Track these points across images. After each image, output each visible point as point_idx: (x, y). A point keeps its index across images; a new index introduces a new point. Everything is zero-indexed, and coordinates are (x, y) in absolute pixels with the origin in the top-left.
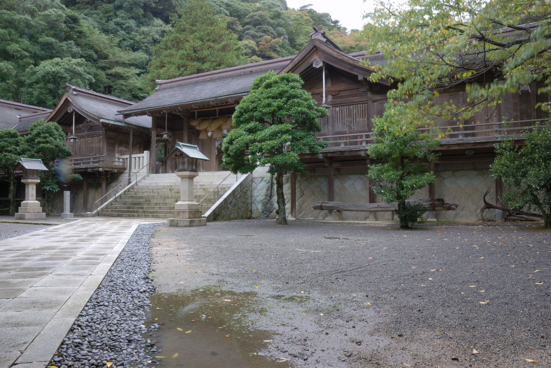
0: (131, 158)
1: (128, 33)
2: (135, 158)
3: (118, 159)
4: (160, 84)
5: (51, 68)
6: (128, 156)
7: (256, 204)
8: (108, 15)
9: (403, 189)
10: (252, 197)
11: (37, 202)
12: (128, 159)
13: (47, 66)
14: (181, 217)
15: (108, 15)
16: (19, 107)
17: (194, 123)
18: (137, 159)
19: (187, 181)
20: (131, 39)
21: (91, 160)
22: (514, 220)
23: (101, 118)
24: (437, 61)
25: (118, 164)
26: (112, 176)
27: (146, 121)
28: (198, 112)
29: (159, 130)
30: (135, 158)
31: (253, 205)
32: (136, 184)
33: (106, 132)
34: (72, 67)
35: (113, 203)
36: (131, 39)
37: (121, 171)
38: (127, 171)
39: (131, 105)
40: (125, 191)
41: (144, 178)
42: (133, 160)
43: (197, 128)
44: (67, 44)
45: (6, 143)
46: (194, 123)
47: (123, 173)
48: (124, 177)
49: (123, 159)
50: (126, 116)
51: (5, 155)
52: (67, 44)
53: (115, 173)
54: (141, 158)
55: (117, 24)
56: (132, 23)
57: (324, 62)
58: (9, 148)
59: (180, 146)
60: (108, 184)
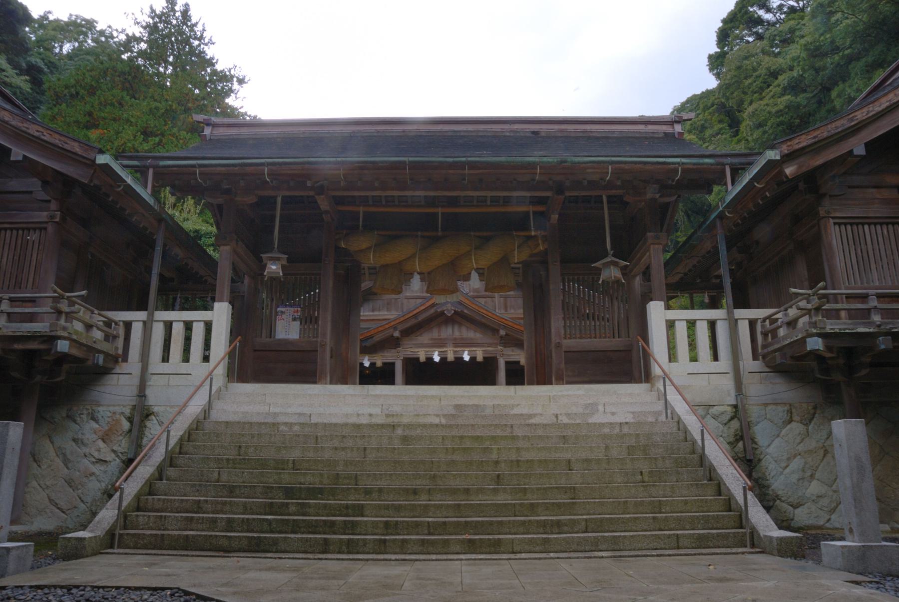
6: (142, 315)
17: (359, 243)
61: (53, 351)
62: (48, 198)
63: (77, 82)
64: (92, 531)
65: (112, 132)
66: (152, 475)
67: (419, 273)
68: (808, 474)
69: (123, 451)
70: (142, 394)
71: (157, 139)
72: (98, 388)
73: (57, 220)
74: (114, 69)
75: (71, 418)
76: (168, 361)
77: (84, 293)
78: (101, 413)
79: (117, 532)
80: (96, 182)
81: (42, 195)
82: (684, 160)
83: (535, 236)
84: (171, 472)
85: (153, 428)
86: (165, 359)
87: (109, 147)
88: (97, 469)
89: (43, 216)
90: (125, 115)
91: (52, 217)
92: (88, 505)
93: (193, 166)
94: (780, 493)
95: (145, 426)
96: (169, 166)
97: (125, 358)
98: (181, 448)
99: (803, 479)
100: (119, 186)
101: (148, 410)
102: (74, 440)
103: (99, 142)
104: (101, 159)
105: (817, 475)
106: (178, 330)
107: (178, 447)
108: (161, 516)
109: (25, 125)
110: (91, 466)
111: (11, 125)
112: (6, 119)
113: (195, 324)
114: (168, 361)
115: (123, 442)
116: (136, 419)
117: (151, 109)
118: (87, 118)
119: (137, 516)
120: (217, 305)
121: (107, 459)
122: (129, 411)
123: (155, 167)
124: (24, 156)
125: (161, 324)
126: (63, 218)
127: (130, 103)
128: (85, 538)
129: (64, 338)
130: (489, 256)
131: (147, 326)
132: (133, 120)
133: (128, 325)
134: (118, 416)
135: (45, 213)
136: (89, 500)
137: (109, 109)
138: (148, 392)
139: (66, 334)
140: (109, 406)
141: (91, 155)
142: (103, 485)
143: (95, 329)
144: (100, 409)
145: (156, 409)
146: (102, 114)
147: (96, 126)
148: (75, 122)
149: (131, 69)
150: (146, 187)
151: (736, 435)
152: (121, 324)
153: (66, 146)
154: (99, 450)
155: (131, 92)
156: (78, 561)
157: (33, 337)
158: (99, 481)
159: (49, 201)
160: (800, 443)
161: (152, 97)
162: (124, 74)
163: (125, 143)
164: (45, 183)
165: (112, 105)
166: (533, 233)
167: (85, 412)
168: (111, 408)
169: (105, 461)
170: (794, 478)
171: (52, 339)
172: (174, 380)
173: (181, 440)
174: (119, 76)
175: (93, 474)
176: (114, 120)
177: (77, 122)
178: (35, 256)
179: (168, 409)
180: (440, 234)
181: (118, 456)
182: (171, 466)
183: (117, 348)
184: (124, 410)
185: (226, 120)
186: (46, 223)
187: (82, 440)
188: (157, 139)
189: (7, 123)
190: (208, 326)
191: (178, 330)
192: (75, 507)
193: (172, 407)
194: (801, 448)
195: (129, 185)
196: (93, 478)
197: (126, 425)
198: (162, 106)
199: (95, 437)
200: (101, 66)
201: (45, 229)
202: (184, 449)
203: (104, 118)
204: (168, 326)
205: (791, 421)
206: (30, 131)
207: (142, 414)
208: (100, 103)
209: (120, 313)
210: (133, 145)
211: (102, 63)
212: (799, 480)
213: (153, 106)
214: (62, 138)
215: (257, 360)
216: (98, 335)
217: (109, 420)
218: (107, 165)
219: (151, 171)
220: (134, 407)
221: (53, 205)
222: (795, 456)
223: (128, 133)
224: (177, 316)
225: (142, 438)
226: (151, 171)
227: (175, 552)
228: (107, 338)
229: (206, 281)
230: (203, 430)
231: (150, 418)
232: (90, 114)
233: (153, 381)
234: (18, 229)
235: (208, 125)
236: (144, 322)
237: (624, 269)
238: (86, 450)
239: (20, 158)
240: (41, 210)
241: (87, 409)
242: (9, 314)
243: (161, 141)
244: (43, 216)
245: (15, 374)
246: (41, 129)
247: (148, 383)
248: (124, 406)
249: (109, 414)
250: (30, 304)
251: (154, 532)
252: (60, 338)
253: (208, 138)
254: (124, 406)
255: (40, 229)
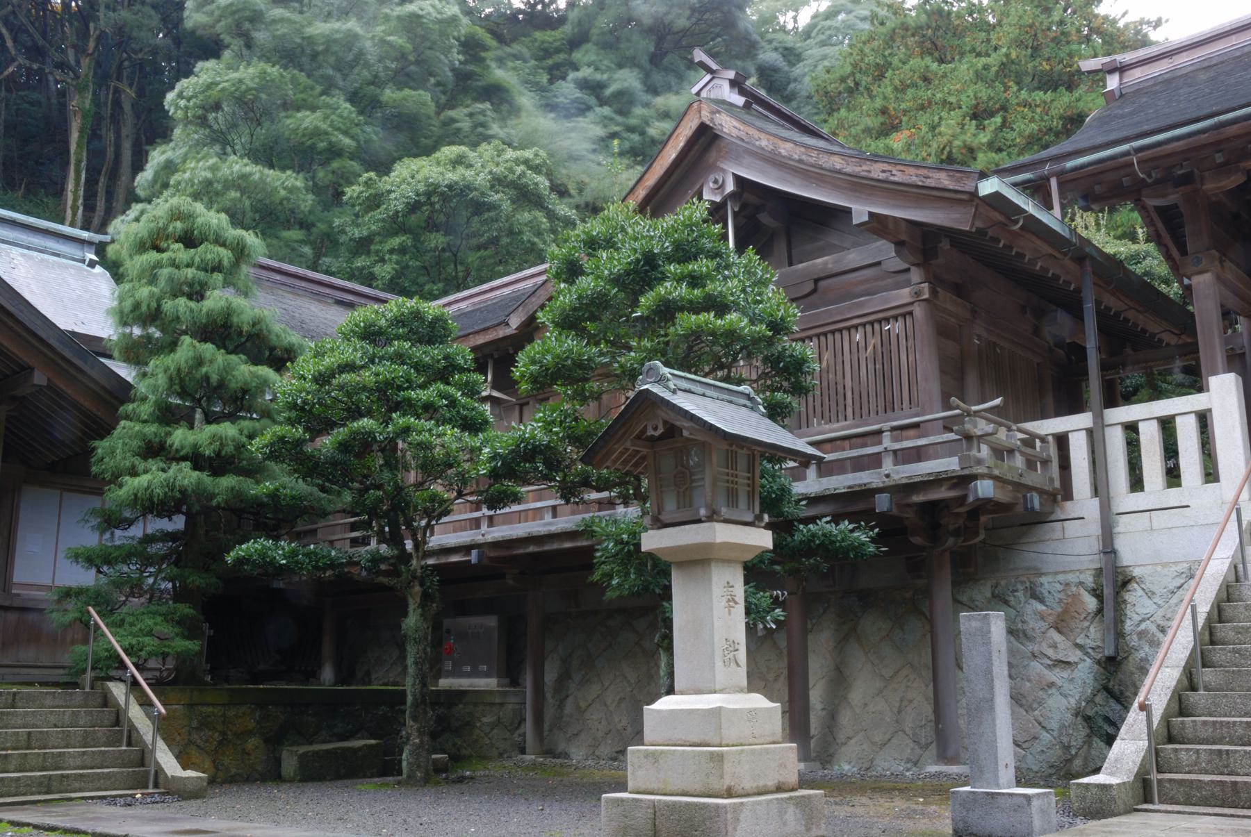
1: (621, 112)
5: (442, 174)
6: (1083, 420)
8: (550, 62)
9: (1193, 688)
11: (759, 701)
13: (410, 176)
15: (550, 62)
16: (351, 298)
20: (631, 129)
21: (887, 442)
24: (963, 423)
34: (511, 170)
36: (631, 129)
44: (471, 115)
45: (401, 370)
51: (407, 430)
52: (471, 115)
55: (585, 85)
56: (628, 79)
58: (423, 395)
61: (971, 499)
62: (906, 266)
63: (855, 65)
64: (1112, 774)
65: (925, 129)
66: (1179, 681)
69: (1094, 644)
70: (1109, 550)
71: (998, 120)
72: (1034, 548)
73: (926, 296)
74: (905, 28)
76: (1142, 489)
77: (998, 401)
78: (1047, 586)
79: (1154, 776)
80: (979, 224)
81: (899, 264)
84: (1207, 676)
85: (1139, 605)
86: (1137, 483)
87: (924, 154)
88: (1056, 676)
89: (904, 295)
90: (939, 96)
91: (917, 294)
92: (1055, 734)
93: (1127, 154)
95: (1125, 602)
96: (1083, 167)
97: (1067, 494)
98: (1211, 634)
100: (1016, 222)
101: (1124, 573)
103: (908, 150)
104: (988, 187)
106: (1150, 437)
107: (1207, 633)
108: (1220, 751)
109: (864, 168)
110: (1046, 672)
111: (846, 174)
112: (838, 167)
113: (1178, 420)
114: (1142, 489)
115: (1092, 629)
116: (1108, 592)
117: (977, 74)
118: (881, 119)
119: (1176, 750)
120: (1214, 381)
121: (1070, 659)
122: (1091, 579)
123: (1059, 174)
124: (871, 214)
125: (1119, 429)
126: (933, 292)
127: (940, 73)
128: (1111, 786)
129: (983, 476)
131: (1095, 438)
132: (952, 99)
133: (1062, 440)
134: (1074, 589)
135: (907, 290)
136: (1054, 725)
137: (910, 92)
138: (1121, 544)
139: (985, 471)
140: (1056, 573)
141: (969, 187)
142: (1073, 701)
143: (1017, 454)
144: (1043, 580)
145: (1136, 572)
146: (903, 106)
147: (895, 128)
148: (864, 131)
149: (929, 16)
150: (1048, 206)
152: (1050, 438)
153: (928, 183)
154: (1054, 646)
155: (936, 54)
156: (1103, 821)
157: (937, 481)
158: (1066, 696)
159: (908, 270)
161: (973, 50)
162: (921, 28)
163: (950, 142)
164: (899, 244)
165: (914, 85)
167: (1020, 587)
168: (1061, 577)
169: (1068, 663)
171: (963, 481)
172: (1160, 519)
173: (1209, 619)
174: (913, 35)
175: (1052, 685)
176: (922, 108)
177: (867, 131)
178: (904, 357)
179: (1159, 568)
181: (1087, 654)
182: (1204, 666)
183: (1052, 480)
184: (1082, 577)
185: (1142, 53)
186: (912, 303)
187: (1024, 632)
188: (998, 120)
189: (839, 172)
190: (1204, 419)
191: (1150, 437)
192: (1035, 738)
193: (1165, 565)
194: (948, 149)
195: (1032, 216)
196: (1054, 690)
197: (1091, 603)
198: (994, 60)
199: (1042, 625)
200: (882, 30)
201: (911, 313)
202: (1219, 635)
203: (905, 112)
204: (1131, 428)
206: (874, 175)
207: (1114, 583)
208: (896, 89)
209: (1044, 421)
210: (964, 142)
211: (882, 24)
213: (980, 66)
214: (921, 172)
216: (1019, 461)
217: (1062, 596)
218: (997, 195)
219: (1054, 183)
220: (1099, 573)
221: (916, 275)
223: (949, 124)
224: (1144, 412)
225: (1123, 622)
226: (1054, 183)
227: (1210, 810)
228: (1031, 464)
229: (1161, 341)
230: (1241, 600)
231: (1129, 587)
232: (884, 111)
233: (1124, 525)
234: (872, 323)
235: (1111, 72)
236: (1090, 432)
238: (1031, 647)
239: (866, 218)
240: (899, 286)
241: (1022, 583)
242: (895, 452)
243: (1004, 120)
244: (904, 295)
245: (917, 540)
246: (886, 167)
247: (1116, 530)
248: (1081, 572)
249: (1060, 587)
250: (911, 432)
251: (1219, 778)
253: (1117, 94)
255: (904, 315)
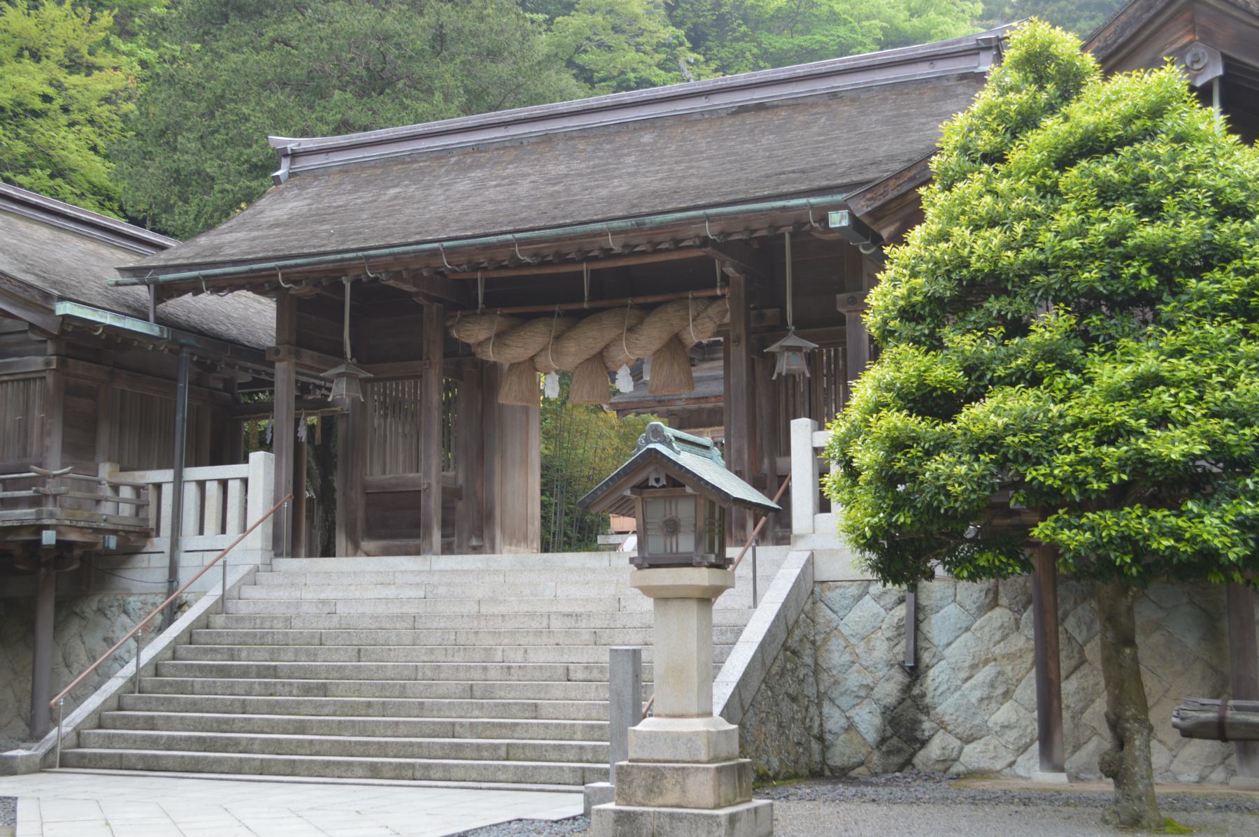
0: (179, 483)
2: (201, 484)
3: (117, 489)
4: (294, 155)
6: (165, 476)
7: (844, 701)
10: (817, 669)
12: (168, 491)
14: (672, 797)
17: (476, 333)
18: (213, 490)
19: (691, 613)
22: (531, 615)
23: (62, 299)
25: (118, 510)
26: (84, 572)
27: (252, 315)
28: (489, 282)
29: (308, 357)
30: (201, 484)
31: (827, 708)
32: (221, 605)
33: (62, 364)
35: (129, 699)
37: (135, 540)
38: (162, 542)
39: (162, 248)
40: (176, 641)
41: (252, 578)
42: (191, 492)
43: (490, 355)
46: (476, 333)
47: (137, 551)
48: (146, 574)
49: (138, 489)
50: (164, 291)
53: (108, 553)
54: (234, 488)
57: (1228, 62)
59: (669, 444)
60: (68, 608)
67: (557, 372)
68: (1000, 690)
75: (101, 611)
82: (813, 200)
83: (723, 296)
94: (946, 718)
99: (989, 698)
102: (105, 639)
105: (1018, 693)
130: (651, 336)
144: (131, 599)
151: (898, 628)
159: (45, 342)
160: (999, 642)
166: (719, 292)
168: (142, 598)
170: (974, 697)
180: (586, 306)
190: (245, 481)
194: (998, 650)
205: (994, 604)
212: (982, 700)
215: (312, 523)
222: (986, 662)
237: (811, 358)
252: (47, 527)
254: (156, 594)
